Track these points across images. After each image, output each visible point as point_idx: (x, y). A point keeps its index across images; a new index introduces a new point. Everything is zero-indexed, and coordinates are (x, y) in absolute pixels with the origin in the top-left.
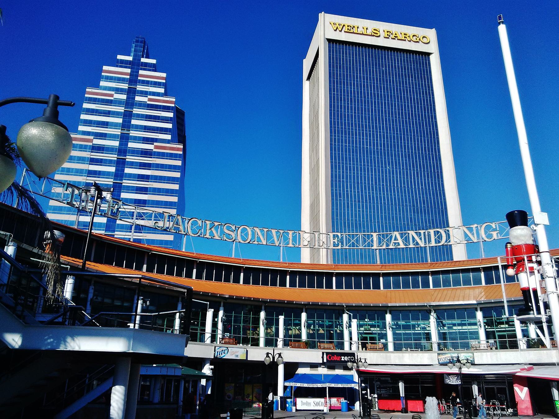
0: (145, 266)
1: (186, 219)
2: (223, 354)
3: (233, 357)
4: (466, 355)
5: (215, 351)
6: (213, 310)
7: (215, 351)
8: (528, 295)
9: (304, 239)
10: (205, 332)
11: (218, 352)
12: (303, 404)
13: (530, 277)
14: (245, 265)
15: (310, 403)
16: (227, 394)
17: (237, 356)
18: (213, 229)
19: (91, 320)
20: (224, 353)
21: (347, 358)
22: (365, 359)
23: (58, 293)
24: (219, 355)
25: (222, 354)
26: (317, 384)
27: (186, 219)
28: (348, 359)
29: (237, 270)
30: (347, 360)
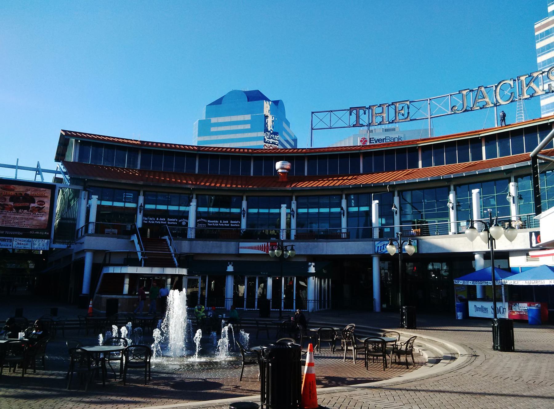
0: (420, 163)
6: (377, 201)
10: (341, 227)
12: (477, 309)
13: (61, 133)
14: (548, 120)
15: (487, 309)
18: (532, 85)
23: (31, 227)
24: (381, 250)
26: (487, 282)
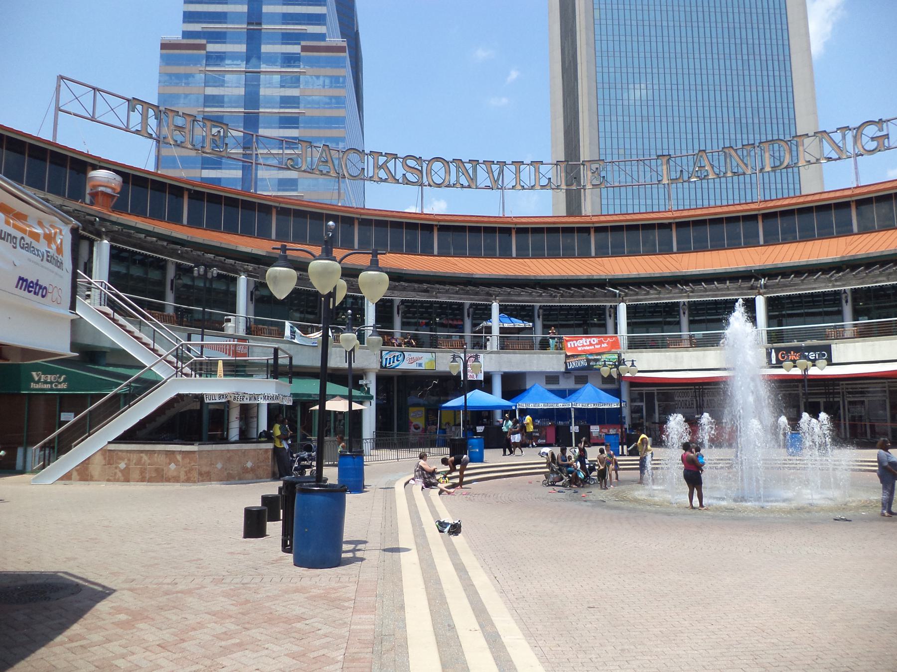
1: (253, 135)
2: (396, 363)
3: (414, 366)
4: (610, 357)
5: (381, 357)
7: (381, 357)
8: (121, 294)
9: (541, 175)
11: (386, 359)
16: (414, 424)
17: (420, 365)
19: (204, 310)
20: (398, 361)
21: (814, 355)
22: (633, 361)
24: (390, 363)
25: (393, 362)
27: (253, 135)
28: (815, 357)
29: (842, 206)
30: (814, 358)
